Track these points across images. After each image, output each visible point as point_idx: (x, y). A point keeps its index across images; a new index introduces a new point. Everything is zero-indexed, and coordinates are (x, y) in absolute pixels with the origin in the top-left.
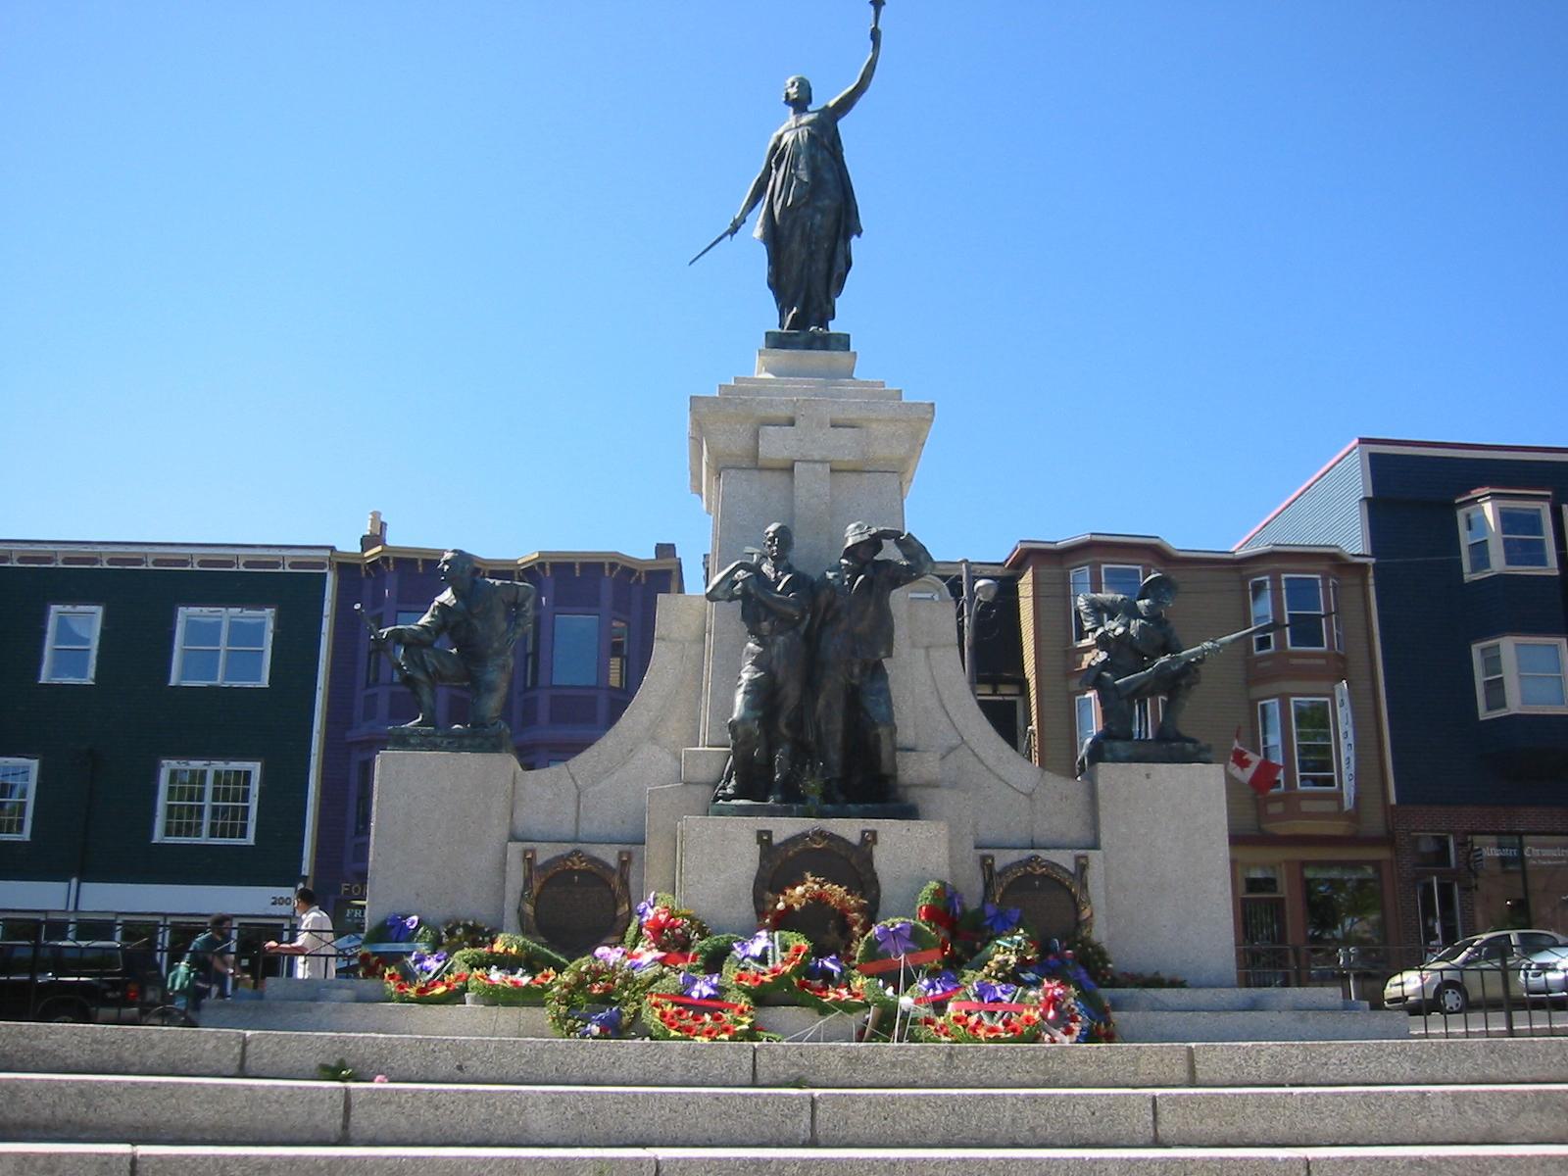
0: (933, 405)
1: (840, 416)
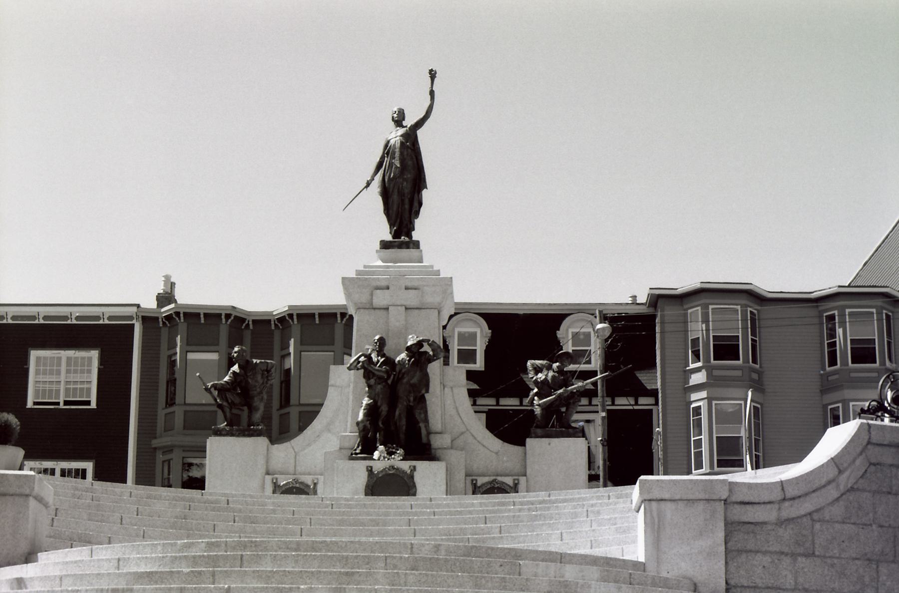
0: (451, 278)
1: (409, 284)
